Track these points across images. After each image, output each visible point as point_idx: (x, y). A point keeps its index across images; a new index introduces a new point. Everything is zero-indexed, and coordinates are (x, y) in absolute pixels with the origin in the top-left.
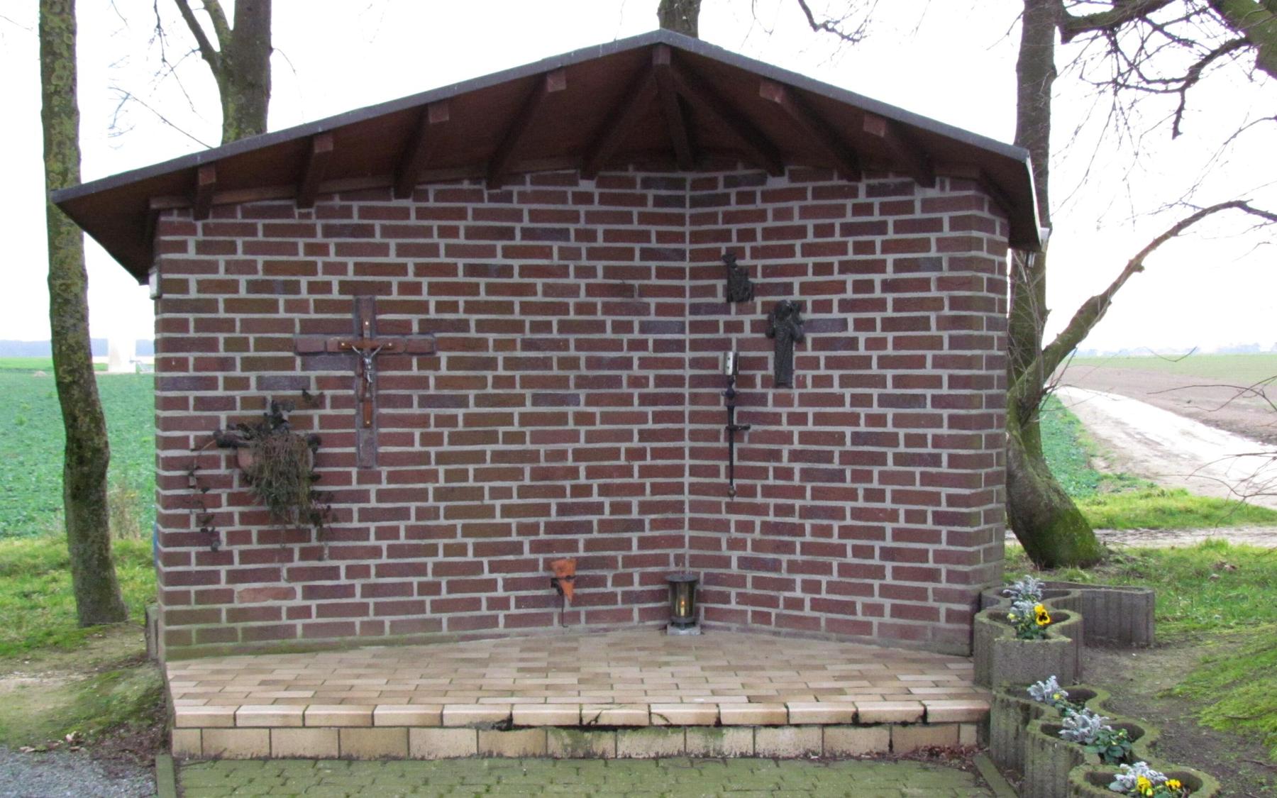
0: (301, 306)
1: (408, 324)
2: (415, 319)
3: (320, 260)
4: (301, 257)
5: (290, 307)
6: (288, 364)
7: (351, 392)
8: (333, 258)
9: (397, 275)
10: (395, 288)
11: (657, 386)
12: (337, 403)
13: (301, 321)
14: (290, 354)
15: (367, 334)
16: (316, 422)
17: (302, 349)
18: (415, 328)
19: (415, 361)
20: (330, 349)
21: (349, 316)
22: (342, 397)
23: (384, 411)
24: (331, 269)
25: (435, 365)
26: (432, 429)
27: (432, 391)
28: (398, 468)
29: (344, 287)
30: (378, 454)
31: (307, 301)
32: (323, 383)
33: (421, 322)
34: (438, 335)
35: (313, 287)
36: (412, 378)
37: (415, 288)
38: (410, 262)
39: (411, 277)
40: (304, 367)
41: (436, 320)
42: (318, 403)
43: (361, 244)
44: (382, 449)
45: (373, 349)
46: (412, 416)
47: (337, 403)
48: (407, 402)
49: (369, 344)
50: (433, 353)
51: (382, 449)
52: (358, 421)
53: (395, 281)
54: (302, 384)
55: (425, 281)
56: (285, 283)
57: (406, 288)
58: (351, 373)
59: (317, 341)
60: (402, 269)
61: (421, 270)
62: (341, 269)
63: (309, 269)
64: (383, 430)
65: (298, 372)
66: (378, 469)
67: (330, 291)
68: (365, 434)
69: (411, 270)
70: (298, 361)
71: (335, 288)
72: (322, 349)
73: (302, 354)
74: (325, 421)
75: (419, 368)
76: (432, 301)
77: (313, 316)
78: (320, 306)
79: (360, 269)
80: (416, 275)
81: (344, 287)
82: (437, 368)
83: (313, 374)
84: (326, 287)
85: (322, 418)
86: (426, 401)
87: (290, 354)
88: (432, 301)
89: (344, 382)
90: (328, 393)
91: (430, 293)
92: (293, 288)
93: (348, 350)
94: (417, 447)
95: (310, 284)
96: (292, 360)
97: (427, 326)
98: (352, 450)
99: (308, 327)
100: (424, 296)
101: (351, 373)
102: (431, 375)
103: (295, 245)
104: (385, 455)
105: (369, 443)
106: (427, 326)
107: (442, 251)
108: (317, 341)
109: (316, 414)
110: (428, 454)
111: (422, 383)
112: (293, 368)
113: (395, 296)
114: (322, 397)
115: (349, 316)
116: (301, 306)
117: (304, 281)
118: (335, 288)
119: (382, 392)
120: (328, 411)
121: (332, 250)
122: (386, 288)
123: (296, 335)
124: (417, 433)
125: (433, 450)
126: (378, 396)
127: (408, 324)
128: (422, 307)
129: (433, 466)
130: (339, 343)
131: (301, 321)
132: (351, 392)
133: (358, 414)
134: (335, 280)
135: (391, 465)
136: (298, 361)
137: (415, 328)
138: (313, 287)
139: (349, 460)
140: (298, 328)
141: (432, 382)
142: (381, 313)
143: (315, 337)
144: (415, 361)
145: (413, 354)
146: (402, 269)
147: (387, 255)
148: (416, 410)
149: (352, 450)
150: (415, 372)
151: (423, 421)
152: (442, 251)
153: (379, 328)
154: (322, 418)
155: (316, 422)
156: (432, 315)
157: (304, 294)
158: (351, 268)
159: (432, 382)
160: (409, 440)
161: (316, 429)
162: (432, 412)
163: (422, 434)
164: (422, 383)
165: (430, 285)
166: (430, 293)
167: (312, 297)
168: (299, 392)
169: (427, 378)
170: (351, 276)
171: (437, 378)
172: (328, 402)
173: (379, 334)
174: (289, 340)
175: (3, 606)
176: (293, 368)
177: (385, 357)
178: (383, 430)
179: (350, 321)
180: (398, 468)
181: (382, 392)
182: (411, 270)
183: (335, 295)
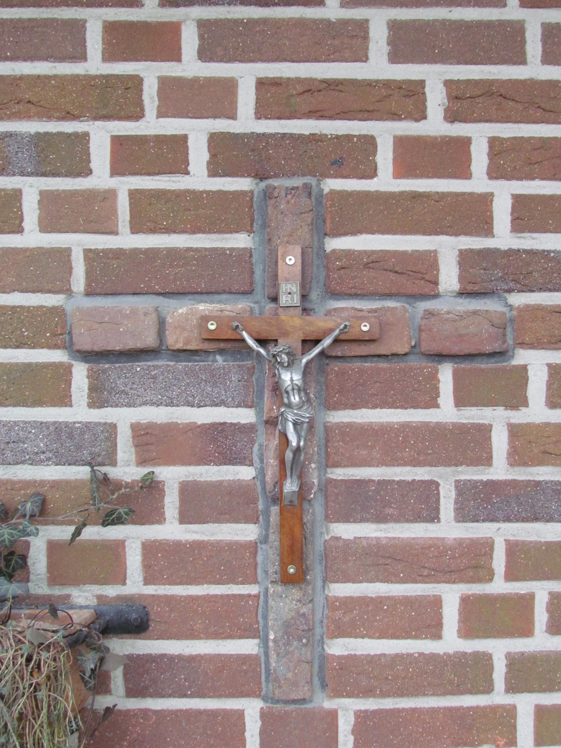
0: (91, 212)
1: (427, 264)
2: (447, 250)
3: (150, 73)
4: (95, 64)
5: (59, 213)
6: (49, 386)
7: (245, 473)
8: (190, 65)
9: (395, 116)
10: (385, 157)
11: (369, 143)
12: (198, 504)
13: (91, 255)
14: (57, 356)
15: (290, 293)
16: (134, 560)
17: (84, 342)
18: (449, 277)
19: (446, 375)
20: (175, 340)
21: (241, 241)
22: (217, 487)
23: (346, 531)
24: (181, 97)
25: (513, 393)
26: (499, 586)
27: (500, 470)
28: (388, 703)
29: (227, 154)
30: (324, 658)
31: (109, 196)
32: (153, 443)
33: (466, 258)
34: (519, 299)
35: (129, 155)
36: (438, 432)
37: (451, 157)
38: (435, 77)
39: (435, 124)
40: (98, 397)
41: (511, 254)
42: (137, 503)
43: (277, 25)
44: (338, 647)
45: (310, 342)
46: (436, 547)
47: (198, 504)
48: (421, 503)
49: (295, 322)
50: (501, 354)
51: (338, 647)
52: (268, 558)
53: (385, 133)
54: (94, 445)
55: (480, 135)
56: (42, 140)
57: (415, 156)
58: (245, 416)
59: (134, 316)
60: (408, 99)
61: (465, 102)
62: (215, 98)
63: (121, 98)
64: (341, 590)
65: (79, 412)
66: (328, 704)
67: (181, 166)
68: (284, 604)
69: (436, 99)
70: (80, 374)
71: (199, 155)
72: (149, 340)
73: (89, 356)
74: (163, 560)
75: (461, 401)
76: (503, 195)
77: (127, 240)
78: (149, 212)
79: (275, 98)
80: (452, 116)
81: (227, 154)
82: (516, 399)
83: (124, 418)
84: (170, 154)
85: (150, 549)
86: (481, 501)
87: (57, 356)
88: (503, 195)
89: (221, 444)
90: (172, 475)
91: (496, 172)
92: (70, 156)
93: (228, 343)
94: (452, 641)
95: (118, 142)
96: (63, 373)
97: (485, 274)
98: (248, 647)
99: (112, 275)
100: (478, 182)
101: (245, 416)
102: (498, 420)
103: (77, 28)
104: (350, 662)
105: (299, 630)
106: (485, 274)
107: (534, 47)
108: (134, 316)
109: (133, 537)
110: (484, 661)
111: (470, 444)
112: (64, 399)
113: (385, 180)
114: (151, 487)
115: (241, 241)
116: (91, 212)
117: (101, 136)
118: (199, 155)
119: (339, 474)
120: (171, 529)
121: (190, 40)
122: (356, 156)
123: (75, 299)
124: (451, 597)
125: (499, 649)
126: (328, 486)
127: (427, 264)
128: (473, 214)
129: (499, 697)
130: (205, 319)
131: (91, 255)
132: (245, 473)
133: (265, 540)
134: (197, 132)
135: (368, 693)
136: (80, 374)
137: (449, 277)
138: (129, 155)
139: (237, 677)
140: (79, 279)
141: (500, 442)
142: (337, 233)
143: (126, 303)
144: (446, 375)
145: (441, 357)
146: (408, 99)
147: (361, 56)
148: (448, 528)
149: (248, 647)
150: (448, 411)
151: (470, 561)
152: (534, 47)
153: (331, 277)
154: (150, 549)
155: (134, 560)
156: (504, 237)
157: (101, 175)
158: (246, 98)
159: (500, 442)
160: (426, 619)
161: (135, 585)
162: (500, 534)
163: (465, 600)
164: (470, 444)
165: (497, 147)
166: (496, 172)
167: (125, 185)
168: (82, 472)
169: (483, 432)
170: (246, 120)
171: (515, 431)
172: (171, 503)
173: (336, 295)
174: (57, 312)
175: (204, 747)
176: (64, 399)
177: (342, 364)
178: (341, 590)
179: (244, 255)
180: (388, 703)
181: (339, 474)
182: (436, 99)
183: (198, 177)
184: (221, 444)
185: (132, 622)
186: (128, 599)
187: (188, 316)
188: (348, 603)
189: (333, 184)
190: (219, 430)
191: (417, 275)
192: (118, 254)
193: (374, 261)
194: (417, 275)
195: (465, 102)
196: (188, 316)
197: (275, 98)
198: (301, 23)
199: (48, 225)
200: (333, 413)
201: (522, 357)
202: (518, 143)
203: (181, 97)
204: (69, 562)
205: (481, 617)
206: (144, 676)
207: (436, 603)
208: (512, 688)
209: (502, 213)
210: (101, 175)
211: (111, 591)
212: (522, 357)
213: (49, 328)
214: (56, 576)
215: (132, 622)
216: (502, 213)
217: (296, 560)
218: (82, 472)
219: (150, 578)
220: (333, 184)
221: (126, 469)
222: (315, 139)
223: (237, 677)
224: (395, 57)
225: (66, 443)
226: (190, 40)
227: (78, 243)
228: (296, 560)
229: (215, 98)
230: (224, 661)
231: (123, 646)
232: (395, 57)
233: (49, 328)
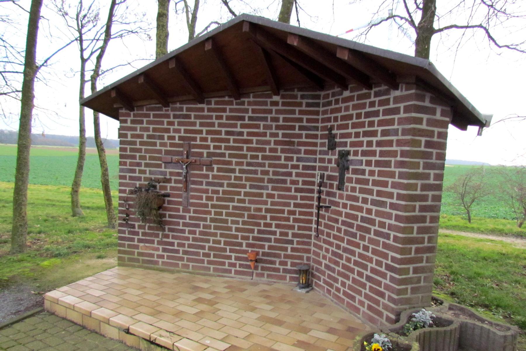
1: (203, 153)
2: (205, 151)
3: (172, 128)
8: (176, 127)
10: (198, 140)
12: (176, 182)
16: (169, 188)
18: (205, 155)
21: (181, 149)
23: (192, 186)
24: (175, 131)
25: (212, 170)
26: (210, 195)
27: (210, 180)
29: (180, 138)
32: (171, 174)
34: (214, 158)
37: (206, 140)
38: (204, 129)
39: (204, 135)
40: (165, 168)
42: (169, 181)
44: (191, 201)
47: (176, 182)
48: (201, 183)
51: (191, 201)
53: (198, 136)
54: (164, 173)
55: (209, 137)
56: (159, 136)
57: (202, 139)
59: (169, 158)
60: (201, 132)
61: (208, 132)
62: (179, 131)
63: (167, 131)
64: (192, 193)
65: (163, 169)
68: (185, 195)
69: (204, 132)
70: (163, 165)
71: (177, 138)
72: (170, 161)
73: (164, 163)
74: (172, 188)
76: (212, 145)
77: (169, 149)
78: (172, 145)
80: (206, 134)
81: (180, 138)
82: (213, 171)
83: (168, 170)
84: (173, 138)
85: (171, 187)
86: (208, 184)
88: (212, 145)
89: (179, 174)
90: (173, 178)
91: (211, 142)
92: (162, 138)
94: (204, 201)
97: (210, 155)
99: (167, 152)
102: (210, 173)
106: (210, 155)
108: (169, 158)
109: (169, 185)
112: (161, 168)
113: (198, 142)
114: (170, 179)
117: (166, 135)
118: (177, 138)
119: (192, 179)
120: (173, 184)
121: (176, 124)
123: (163, 155)
125: (210, 203)
127: (203, 153)
128: (208, 147)
134: (177, 135)
136: (163, 165)
137: (205, 155)
138: (170, 138)
139: (179, 203)
141: (211, 176)
145: (204, 165)
146: (201, 132)
148: (204, 187)
150: (204, 172)
151: (207, 191)
154: (171, 187)
155: (169, 188)
156: (212, 150)
157: (166, 140)
159: (211, 176)
160: (201, 198)
161: (168, 191)
162: (210, 188)
164: (207, 176)
166: (211, 142)
169: (209, 175)
170: (182, 134)
172: (173, 181)
176: (161, 168)
178: (192, 193)
181: (192, 179)
182: (204, 132)
183: (177, 141)
184: (179, 174)
185: (168, 195)
186: (167, 193)
187: (175, 158)
188: (192, 195)
189: (192, 143)
190: (178, 172)
191: (201, 154)
192: (167, 150)
193: (197, 152)
194: (201, 154)
195: (208, 132)
196: (175, 158)
197: (186, 131)
198: (189, 122)
199: (160, 146)
200: (429, 99)
201: (214, 166)
202: (214, 138)
203: (175, 131)
204: (162, 188)
205: (208, 198)
206: (169, 202)
207: (202, 196)
208: (211, 208)
209: (212, 147)
210: (166, 140)
211: (166, 192)
212: (214, 166)
213: (159, 159)
214: (160, 189)
215: (168, 195)
216: (212, 147)
217: (186, 189)
218: (162, 177)
219: (170, 190)
220: (192, 143)
221: (168, 177)
222: (190, 137)
223: (179, 203)
224: (167, 125)
225: (162, 173)
226: (176, 124)
227: (163, 148)
228: (186, 189)
229: (179, 131)
230: (177, 201)
231: (167, 199)
232: (167, 125)
233: (159, 159)
